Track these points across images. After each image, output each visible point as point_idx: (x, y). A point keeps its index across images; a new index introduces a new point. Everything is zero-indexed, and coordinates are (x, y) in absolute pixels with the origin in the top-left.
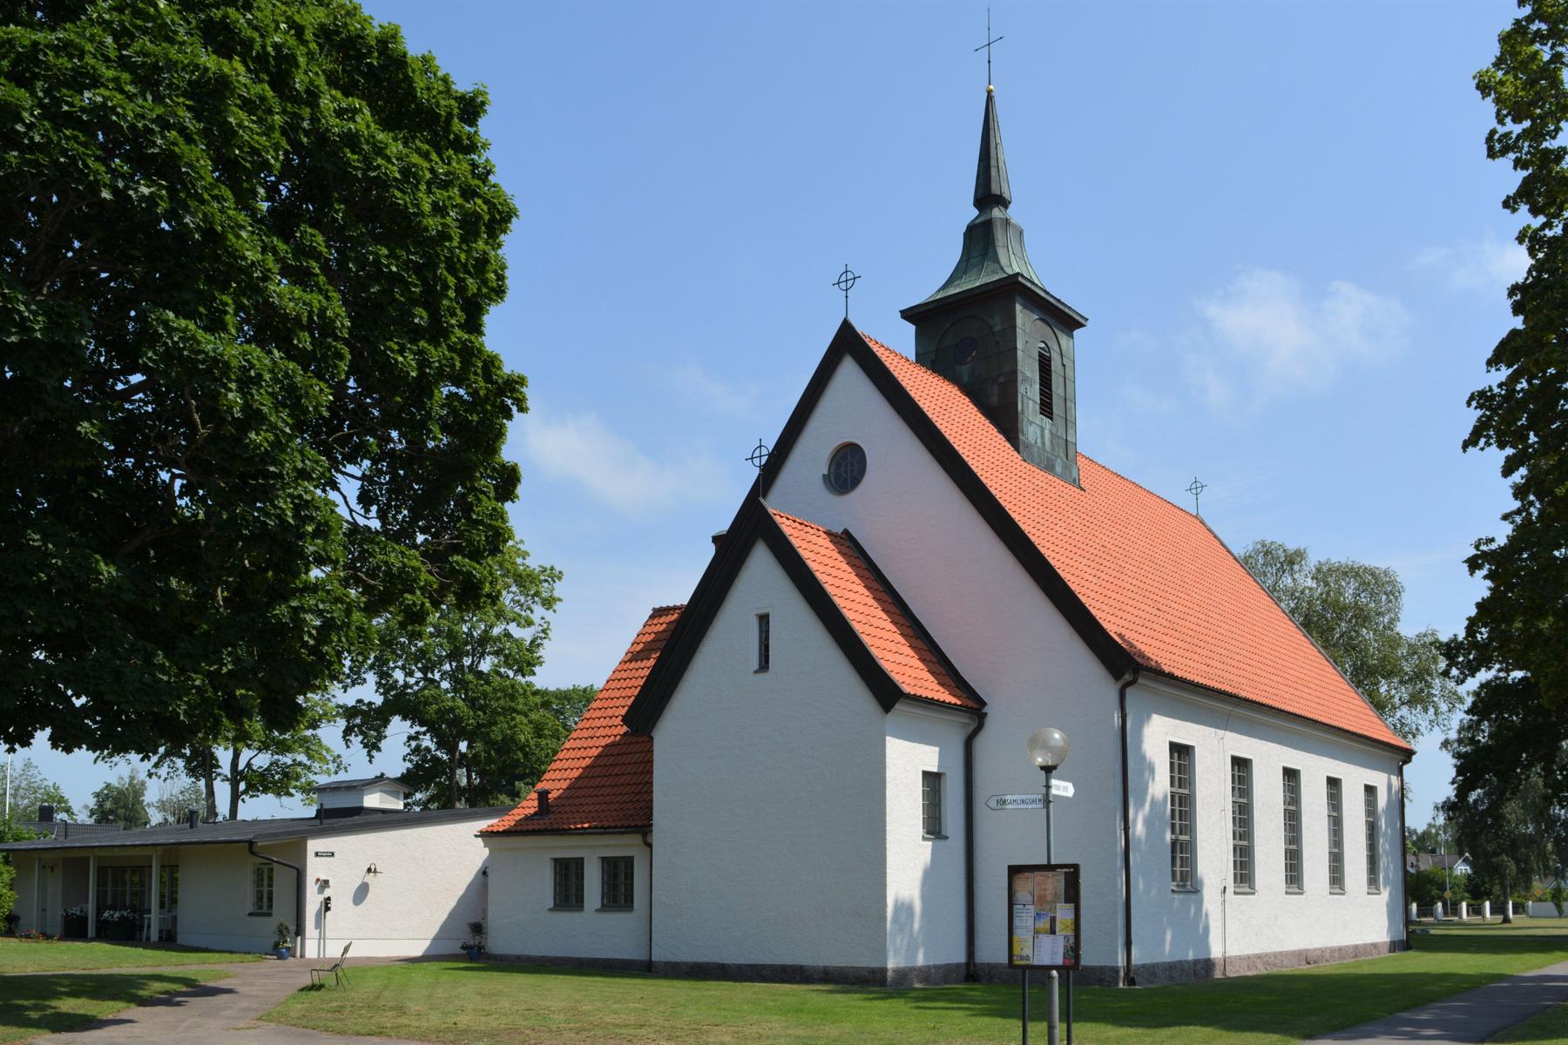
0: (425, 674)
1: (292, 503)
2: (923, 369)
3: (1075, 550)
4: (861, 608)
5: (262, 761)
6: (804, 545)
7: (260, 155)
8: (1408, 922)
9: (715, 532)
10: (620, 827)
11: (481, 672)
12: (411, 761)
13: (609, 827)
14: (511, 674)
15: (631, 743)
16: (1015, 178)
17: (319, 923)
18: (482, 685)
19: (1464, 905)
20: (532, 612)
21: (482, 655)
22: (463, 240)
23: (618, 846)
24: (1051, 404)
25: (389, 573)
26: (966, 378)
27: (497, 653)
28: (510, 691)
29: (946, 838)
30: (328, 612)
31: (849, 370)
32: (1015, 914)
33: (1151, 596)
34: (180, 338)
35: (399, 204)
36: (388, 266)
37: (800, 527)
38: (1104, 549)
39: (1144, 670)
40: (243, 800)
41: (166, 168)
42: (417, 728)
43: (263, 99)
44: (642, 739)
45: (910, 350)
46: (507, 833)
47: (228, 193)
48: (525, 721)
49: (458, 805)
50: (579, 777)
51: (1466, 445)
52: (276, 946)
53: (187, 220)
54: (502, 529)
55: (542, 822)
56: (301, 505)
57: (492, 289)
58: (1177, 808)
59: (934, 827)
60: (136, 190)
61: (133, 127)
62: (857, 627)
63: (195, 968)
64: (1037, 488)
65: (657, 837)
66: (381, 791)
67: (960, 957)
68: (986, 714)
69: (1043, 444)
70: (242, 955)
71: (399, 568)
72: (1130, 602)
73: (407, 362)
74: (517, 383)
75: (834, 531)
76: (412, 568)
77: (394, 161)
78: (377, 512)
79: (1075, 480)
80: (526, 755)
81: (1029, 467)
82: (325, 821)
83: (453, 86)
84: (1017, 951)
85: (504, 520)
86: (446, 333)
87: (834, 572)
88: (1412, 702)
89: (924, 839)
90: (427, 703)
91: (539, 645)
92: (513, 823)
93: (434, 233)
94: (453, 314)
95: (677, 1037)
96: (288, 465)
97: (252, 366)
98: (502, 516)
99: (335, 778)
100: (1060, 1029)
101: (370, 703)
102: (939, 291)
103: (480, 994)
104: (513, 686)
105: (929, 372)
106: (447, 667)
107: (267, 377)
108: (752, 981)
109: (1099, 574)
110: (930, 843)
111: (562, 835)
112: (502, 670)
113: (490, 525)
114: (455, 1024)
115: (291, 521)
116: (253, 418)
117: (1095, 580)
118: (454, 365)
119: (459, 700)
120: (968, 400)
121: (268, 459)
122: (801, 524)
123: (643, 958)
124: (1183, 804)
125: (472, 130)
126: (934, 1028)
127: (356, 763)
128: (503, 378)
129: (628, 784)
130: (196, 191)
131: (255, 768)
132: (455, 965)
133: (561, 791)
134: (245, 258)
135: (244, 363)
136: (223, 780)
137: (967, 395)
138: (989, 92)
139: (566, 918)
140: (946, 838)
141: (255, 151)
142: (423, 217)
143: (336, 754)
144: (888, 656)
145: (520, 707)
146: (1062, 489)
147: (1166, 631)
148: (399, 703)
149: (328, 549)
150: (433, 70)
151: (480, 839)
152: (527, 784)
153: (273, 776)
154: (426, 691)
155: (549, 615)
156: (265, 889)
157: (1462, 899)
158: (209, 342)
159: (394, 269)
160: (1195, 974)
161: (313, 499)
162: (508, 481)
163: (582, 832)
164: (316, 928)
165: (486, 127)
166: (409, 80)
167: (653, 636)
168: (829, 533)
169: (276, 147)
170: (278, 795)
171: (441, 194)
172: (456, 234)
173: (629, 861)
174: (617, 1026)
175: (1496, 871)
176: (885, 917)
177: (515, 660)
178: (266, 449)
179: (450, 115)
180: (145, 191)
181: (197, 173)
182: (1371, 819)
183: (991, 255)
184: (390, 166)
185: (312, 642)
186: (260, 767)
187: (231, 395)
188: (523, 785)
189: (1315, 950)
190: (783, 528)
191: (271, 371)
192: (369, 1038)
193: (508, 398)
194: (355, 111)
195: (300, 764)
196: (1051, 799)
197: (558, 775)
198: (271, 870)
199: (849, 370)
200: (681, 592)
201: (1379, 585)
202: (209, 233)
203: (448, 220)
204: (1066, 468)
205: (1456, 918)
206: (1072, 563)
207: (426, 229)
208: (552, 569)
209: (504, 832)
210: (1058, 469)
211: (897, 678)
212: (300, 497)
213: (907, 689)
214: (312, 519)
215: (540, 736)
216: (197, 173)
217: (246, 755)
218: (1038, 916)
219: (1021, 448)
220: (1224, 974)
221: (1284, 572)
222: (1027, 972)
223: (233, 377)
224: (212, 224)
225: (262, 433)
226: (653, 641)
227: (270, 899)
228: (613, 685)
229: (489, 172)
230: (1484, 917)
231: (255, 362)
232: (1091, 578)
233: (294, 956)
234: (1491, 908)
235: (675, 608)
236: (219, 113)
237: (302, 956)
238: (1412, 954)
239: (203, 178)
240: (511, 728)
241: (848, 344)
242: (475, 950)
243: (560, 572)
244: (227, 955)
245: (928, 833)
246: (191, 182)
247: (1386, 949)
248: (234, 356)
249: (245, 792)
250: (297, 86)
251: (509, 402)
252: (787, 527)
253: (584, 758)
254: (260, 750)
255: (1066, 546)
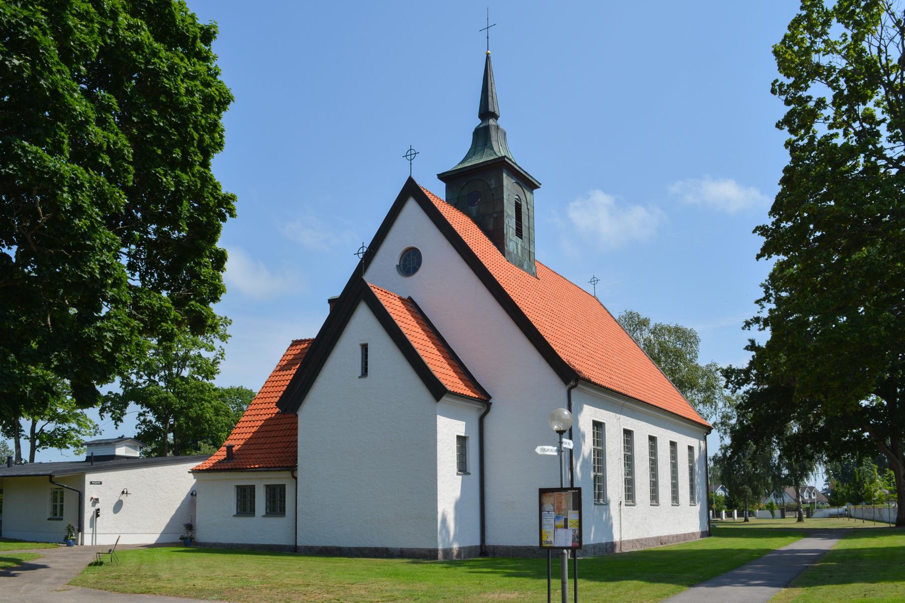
0: (149, 378)
1: (99, 264)
2: (452, 207)
3: (539, 312)
4: (422, 342)
5: (50, 427)
6: (388, 305)
7: (85, 47)
8: (709, 522)
9: (331, 296)
10: (273, 468)
11: (183, 377)
12: (140, 428)
13: (271, 467)
14: (200, 378)
15: (281, 418)
16: (501, 103)
17: (93, 524)
18: (184, 385)
19: (724, 511)
20: (213, 343)
21: (184, 366)
22: (204, 111)
23: (276, 478)
24: (522, 230)
25: (152, 310)
26: (474, 214)
27: (193, 366)
28: (201, 388)
29: (470, 474)
30: (120, 332)
31: (412, 205)
32: (543, 517)
33: (579, 339)
34: (32, 157)
35: (166, 87)
36: (157, 122)
37: (385, 294)
38: (552, 312)
39: (581, 379)
40: (38, 451)
41: (31, 48)
42: (145, 409)
43: (88, 12)
44: (288, 416)
45: (442, 194)
46: (208, 471)
47: (67, 69)
48: (210, 406)
49: (168, 454)
50: (251, 438)
51: (759, 257)
52: (66, 539)
53: (42, 82)
54: (219, 285)
55: (229, 464)
56: (104, 266)
57: (216, 143)
58: (596, 457)
59: (463, 468)
60: (10, 62)
61: (9, 22)
62: (420, 353)
63: (18, 552)
64: (516, 277)
65: (300, 473)
66: (126, 446)
67: (477, 542)
68: (491, 403)
69: (517, 252)
70: (45, 544)
71: (158, 307)
72: (569, 342)
73: (168, 181)
74: (231, 199)
75: (403, 297)
76: (166, 307)
77: (164, 60)
78: (140, 276)
79: (534, 273)
80: (209, 425)
81: (511, 265)
82: (94, 463)
83: (197, 21)
84: (544, 539)
85: (220, 281)
86: (192, 165)
87: (405, 321)
88: (704, 402)
89: (458, 474)
90: (151, 394)
91: (219, 362)
92: (211, 465)
93: (186, 106)
94: (196, 155)
95: (332, 591)
96: (98, 241)
97: (78, 178)
98: (218, 278)
99: (94, 438)
100: (570, 584)
101: (116, 394)
102: (459, 164)
103: (201, 567)
104: (202, 386)
105: (455, 209)
106: (163, 373)
107: (87, 185)
108: (359, 557)
109: (552, 325)
110: (461, 477)
111: (242, 472)
112: (196, 376)
113: (212, 283)
114: (194, 585)
115: (98, 276)
116: (78, 210)
117: (551, 329)
118: (196, 186)
119: (170, 393)
120: (476, 226)
121: (86, 236)
122: (385, 292)
123: (290, 544)
124: (600, 455)
125: (207, 48)
126: (480, 584)
127: (107, 428)
128: (222, 196)
129: (281, 442)
130: (48, 66)
131: (45, 431)
132: (174, 549)
133: (240, 446)
134: (75, 110)
135: (73, 176)
136: (25, 439)
137: (476, 223)
138: (488, 54)
139: (244, 521)
140: (470, 474)
141: (82, 44)
142: (180, 96)
143: (95, 424)
144: (437, 369)
145: (206, 397)
146: (528, 278)
147: (589, 358)
148: (133, 394)
149: (121, 294)
150: (184, 10)
151: (192, 474)
152: (205, 443)
153: (57, 437)
154: (151, 387)
155: (223, 344)
156: (58, 504)
157: (723, 509)
158: (51, 161)
159: (162, 124)
160: (606, 551)
161: (112, 263)
162: (220, 259)
163: (255, 470)
164: (91, 527)
165: (216, 47)
166: (172, 14)
167: (292, 356)
168: (400, 298)
169: (95, 42)
170: (60, 447)
171: (190, 83)
172: (200, 107)
173: (282, 488)
174: (293, 585)
175: (741, 494)
176: (437, 519)
177: (204, 370)
178: (85, 230)
179: (195, 38)
180: (17, 62)
181: (49, 54)
182: (691, 465)
183: (488, 145)
184: (162, 64)
185: (109, 350)
186: (49, 431)
187: (65, 195)
188: (202, 444)
189: (665, 536)
190: (376, 294)
191: (89, 182)
192: (142, 595)
193: (224, 208)
194: (138, 27)
195: (73, 429)
196: (563, 450)
197: (237, 436)
198: (62, 493)
199: (412, 205)
200: (311, 331)
201: (685, 337)
202: (55, 92)
203: (195, 99)
204: (530, 267)
205: (719, 519)
206: (538, 319)
207: (182, 103)
208: (226, 318)
209: (206, 469)
210: (525, 267)
211: (444, 382)
212: (104, 261)
213: (449, 388)
214: (111, 275)
215: (218, 415)
216: (49, 54)
217: (40, 424)
218: (557, 518)
219: (506, 254)
220: (621, 550)
221: (637, 329)
222: (550, 550)
223: (66, 184)
224: (56, 86)
225: (83, 220)
226: (293, 359)
227: (62, 509)
228: (270, 384)
229: (217, 74)
230: (734, 518)
231: (80, 175)
232: (548, 327)
233: (77, 544)
234: (737, 514)
235: (305, 341)
236: (62, 18)
237: (82, 544)
238: (712, 538)
239: (52, 58)
240: (201, 410)
241: (411, 190)
242: (188, 540)
243: (231, 320)
244: (35, 544)
245: (459, 471)
246: (45, 59)
247: (698, 536)
248: (67, 171)
249: (40, 446)
250: (105, 6)
251: (224, 211)
252: (379, 295)
253: (253, 427)
254: (49, 420)
255: (534, 309)
